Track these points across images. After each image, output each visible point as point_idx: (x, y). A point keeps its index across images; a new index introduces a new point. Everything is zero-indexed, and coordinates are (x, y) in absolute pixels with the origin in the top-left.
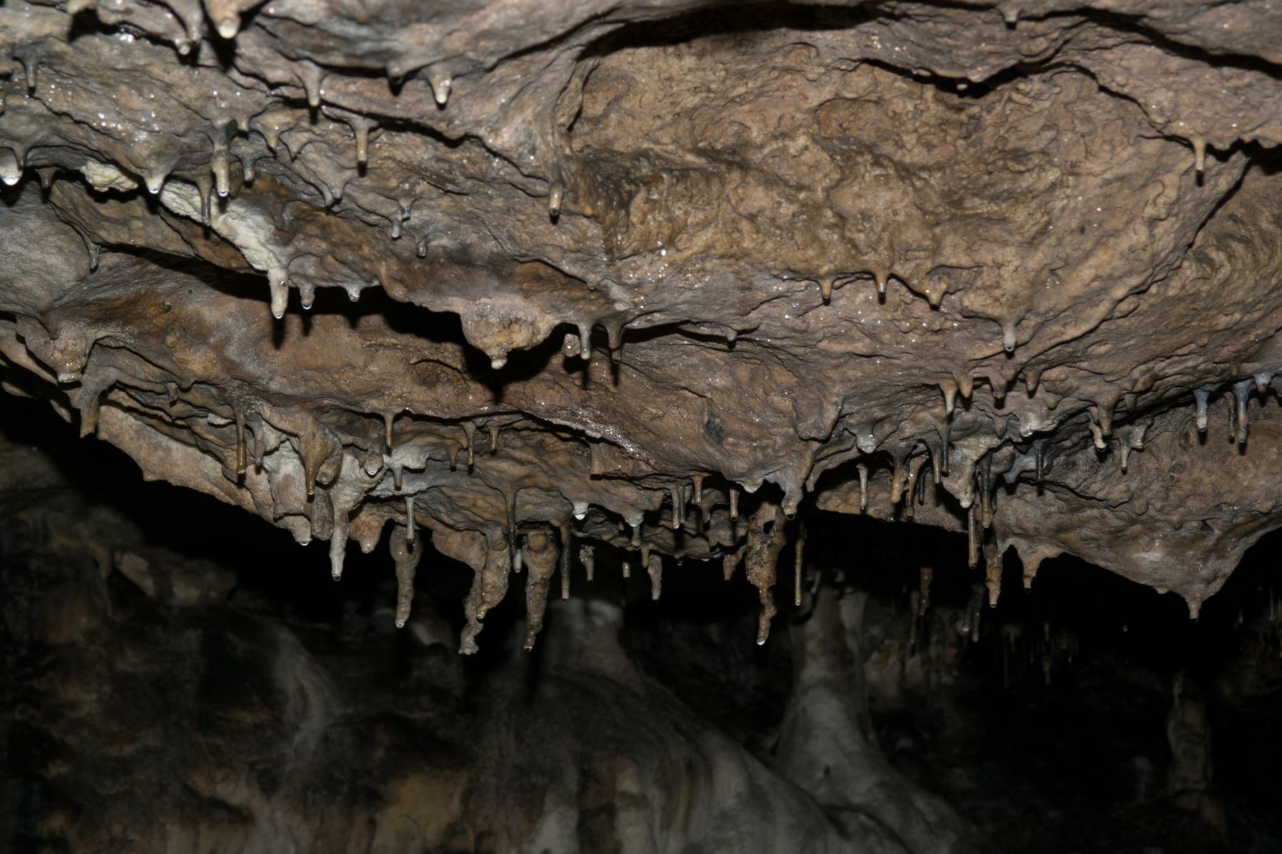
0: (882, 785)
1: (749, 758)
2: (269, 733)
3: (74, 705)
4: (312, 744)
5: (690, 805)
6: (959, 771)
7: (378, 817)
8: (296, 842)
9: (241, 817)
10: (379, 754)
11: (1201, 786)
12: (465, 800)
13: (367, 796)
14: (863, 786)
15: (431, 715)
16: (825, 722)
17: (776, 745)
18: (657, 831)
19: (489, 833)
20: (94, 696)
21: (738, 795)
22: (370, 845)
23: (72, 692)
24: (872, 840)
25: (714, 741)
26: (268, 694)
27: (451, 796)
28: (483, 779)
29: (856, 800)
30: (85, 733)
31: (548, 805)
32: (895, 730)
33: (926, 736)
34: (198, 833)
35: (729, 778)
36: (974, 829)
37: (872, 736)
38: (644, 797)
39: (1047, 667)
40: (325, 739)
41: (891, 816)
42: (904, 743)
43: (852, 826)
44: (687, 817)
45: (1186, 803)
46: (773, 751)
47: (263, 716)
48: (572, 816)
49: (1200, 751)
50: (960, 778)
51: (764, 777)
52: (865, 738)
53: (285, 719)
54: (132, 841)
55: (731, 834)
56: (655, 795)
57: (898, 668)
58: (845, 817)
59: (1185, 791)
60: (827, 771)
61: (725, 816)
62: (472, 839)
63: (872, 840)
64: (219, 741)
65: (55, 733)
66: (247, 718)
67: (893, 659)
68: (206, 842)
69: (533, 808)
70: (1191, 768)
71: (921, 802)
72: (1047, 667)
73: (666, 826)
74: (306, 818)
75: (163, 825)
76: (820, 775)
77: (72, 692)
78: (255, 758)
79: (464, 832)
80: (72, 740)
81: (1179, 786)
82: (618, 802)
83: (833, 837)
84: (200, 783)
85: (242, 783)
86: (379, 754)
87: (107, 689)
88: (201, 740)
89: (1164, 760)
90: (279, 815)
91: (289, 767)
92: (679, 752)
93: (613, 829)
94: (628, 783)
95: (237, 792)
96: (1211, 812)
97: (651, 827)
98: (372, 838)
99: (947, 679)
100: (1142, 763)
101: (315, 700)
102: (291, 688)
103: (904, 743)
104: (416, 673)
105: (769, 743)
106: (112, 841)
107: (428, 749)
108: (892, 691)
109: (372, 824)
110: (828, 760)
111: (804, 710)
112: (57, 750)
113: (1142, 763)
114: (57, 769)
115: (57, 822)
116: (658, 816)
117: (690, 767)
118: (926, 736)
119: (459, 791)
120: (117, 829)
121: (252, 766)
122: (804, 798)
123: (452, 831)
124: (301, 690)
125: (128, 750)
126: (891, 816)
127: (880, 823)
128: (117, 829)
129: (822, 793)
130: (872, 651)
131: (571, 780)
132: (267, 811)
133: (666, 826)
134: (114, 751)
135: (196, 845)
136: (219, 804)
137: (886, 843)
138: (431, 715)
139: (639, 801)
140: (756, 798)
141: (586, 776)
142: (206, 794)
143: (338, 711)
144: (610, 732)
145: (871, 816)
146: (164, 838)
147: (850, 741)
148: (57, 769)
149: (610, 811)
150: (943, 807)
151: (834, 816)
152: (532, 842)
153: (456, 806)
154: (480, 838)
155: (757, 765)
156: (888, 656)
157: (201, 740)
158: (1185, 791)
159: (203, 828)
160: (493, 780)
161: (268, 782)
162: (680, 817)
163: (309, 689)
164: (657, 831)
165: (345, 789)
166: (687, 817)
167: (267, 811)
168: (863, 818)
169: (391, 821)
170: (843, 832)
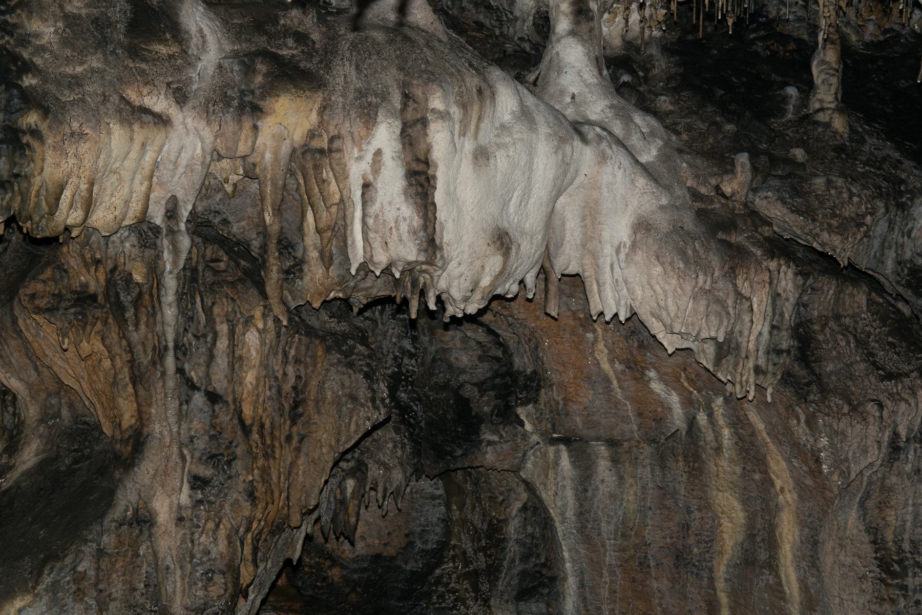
0: (612, 107)
1: (520, 87)
2: (179, 61)
3: (37, 36)
4: (210, 71)
5: (480, 119)
6: (663, 98)
7: (259, 123)
8: (202, 140)
9: (162, 121)
10: (259, 79)
11: (832, 106)
12: (321, 112)
13: (251, 108)
14: (598, 107)
15: (295, 52)
16: (573, 63)
17: (537, 79)
18: (456, 137)
19: (339, 137)
20: (52, 29)
21: (513, 113)
22: (254, 143)
23: (35, 25)
24: (604, 145)
25: (496, 74)
26: (177, 34)
27: (311, 110)
28: (333, 98)
29: (593, 117)
30: (47, 56)
31: (380, 117)
32: (622, 69)
33: (641, 74)
34: (132, 131)
35: (507, 98)
36: (674, 138)
37: (605, 72)
38: (448, 113)
39: (730, 22)
40: (220, 67)
41: (617, 128)
42: (626, 78)
43: (591, 136)
44: (477, 127)
45: (821, 117)
46: (535, 83)
47: (174, 49)
48: (397, 125)
49: (834, 80)
50: (664, 103)
51: (530, 100)
52: (601, 74)
53: (190, 52)
54: (87, 134)
55: (508, 139)
56: (456, 112)
57: (622, 25)
58: (585, 129)
59: (822, 109)
60: (573, 97)
61: (503, 127)
62: (326, 141)
63: (604, 145)
64: (144, 66)
65: (26, 55)
66: (163, 50)
67: (619, 18)
68: (139, 137)
69: (369, 117)
70: (826, 91)
71: (638, 118)
72: (730, 22)
73: (463, 134)
74: (209, 123)
75: (109, 124)
76: (568, 100)
77: (35, 25)
78: (170, 79)
79: (321, 136)
80: (38, 61)
81: (817, 106)
82: (430, 116)
83: (577, 143)
84: (132, 95)
85: (162, 97)
86: (259, 79)
87: (60, 24)
88: (131, 65)
89: (808, 86)
90: (189, 120)
91: (195, 87)
92: (472, 81)
93: (426, 135)
94: (437, 102)
95: (159, 103)
96: (839, 123)
97: (452, 134)
98: (256, 138)
99: (656, 33)
100: (792, 91)
101: (210, 38)
102: (193, 30)
103: (626, 78)
104: (282, 22)
105: (532, 78)
106: (72, 134)
107: (294, 75)
108: (617, 42)
109: (255, 128)
110: (573, 90)
111: (557, 54)
112: (27, 67)
113: (792, 91)
114: (29, 81)
115: (32, 119)
116: (457, 126)
117: (480, 92)
118: (641, 74)
119: (316, 107)
120: (75, 125)
121: (169, 85)
122: (558, 115)
123: (312, 135)
124: (201, 31)
125: (79, 69)
126: (617, 128)
127: (610, 133)
128: (75, 125)
129: (570, 112)
130: (604, 12)
131: (396, 99)
132: (180, 117)
133: (463, 134)
134: (69, 70)
135: (132, 139)
136: (146, 111)
137: (614, 146)
138: (295, 52)
139: (444, 116)
140: (525, 115)
141: (406, 97)
142: (137, 103)
143: (228, 47)
144: (423, 66)
145: (604, 129)
146: (109, 133)
147: (590, 75)
148: (29, 81)
149: (424, 122)
150: (654, 122)
151: (578, 129)
152: (369, 143)
153: (314, 117)
154: (331, 140)
155: (526, 91)
156: (615, 17)
157: (131, 65)
158: (822, 109)
159: (136, 127)
160: (341, 99)
161: (181, 97)
162: (473, 127)
163: (206, 31)
164: (456, 137)
165: (235, 103)
166: (477, 127)
167: (180, 117)
168: (598, 129)
169: (268, 127)
170: (584, 139)
